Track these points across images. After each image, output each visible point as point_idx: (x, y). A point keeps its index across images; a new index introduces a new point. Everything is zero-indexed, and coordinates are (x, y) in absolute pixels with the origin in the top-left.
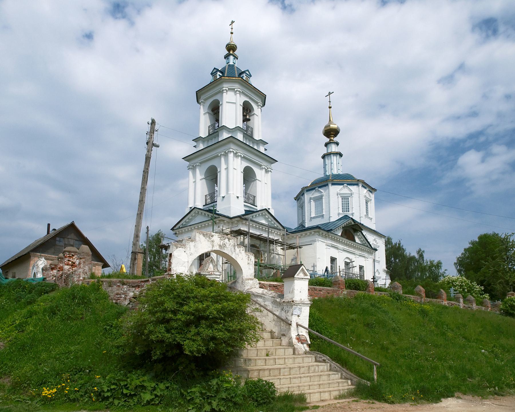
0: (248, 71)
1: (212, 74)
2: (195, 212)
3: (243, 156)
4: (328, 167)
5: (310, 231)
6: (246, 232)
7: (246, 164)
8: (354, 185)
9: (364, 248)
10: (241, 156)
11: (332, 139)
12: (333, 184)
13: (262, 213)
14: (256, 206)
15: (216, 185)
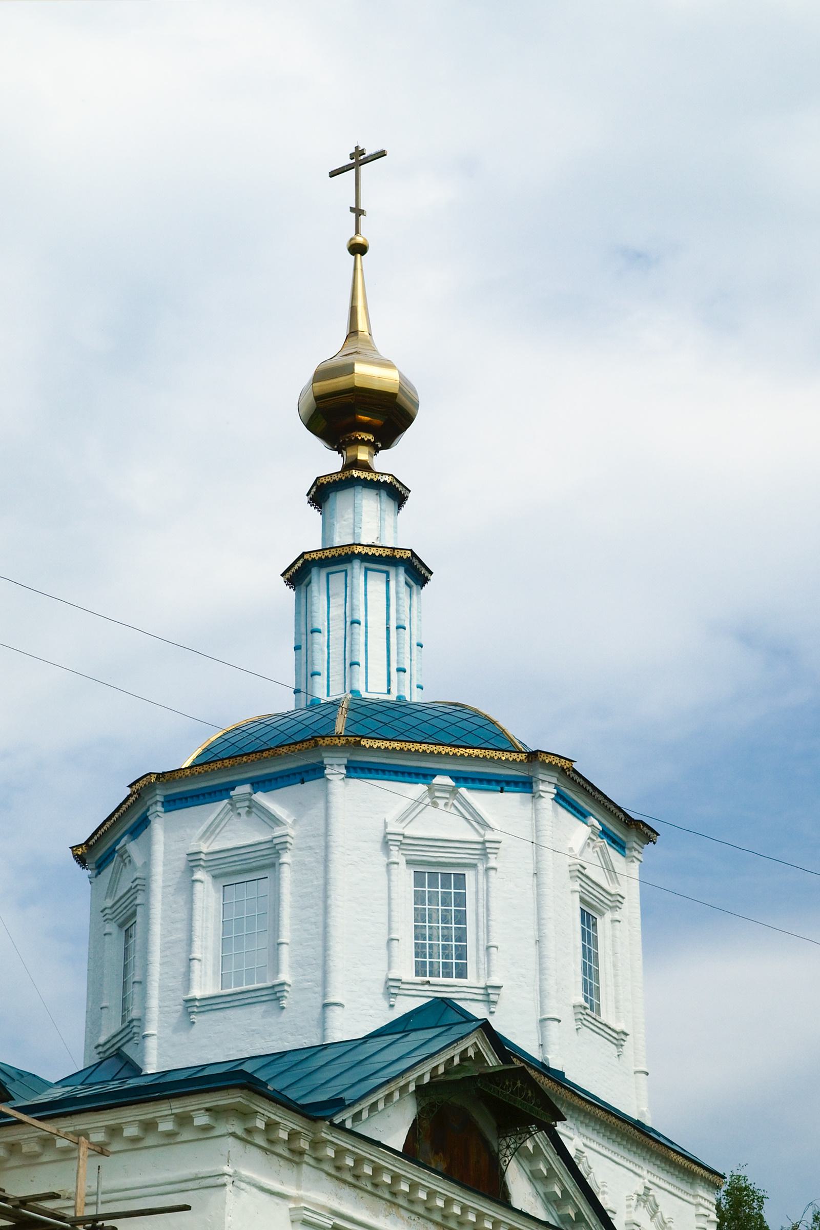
8: (502, 784)
11: (363, 454)
12: (355, 770)
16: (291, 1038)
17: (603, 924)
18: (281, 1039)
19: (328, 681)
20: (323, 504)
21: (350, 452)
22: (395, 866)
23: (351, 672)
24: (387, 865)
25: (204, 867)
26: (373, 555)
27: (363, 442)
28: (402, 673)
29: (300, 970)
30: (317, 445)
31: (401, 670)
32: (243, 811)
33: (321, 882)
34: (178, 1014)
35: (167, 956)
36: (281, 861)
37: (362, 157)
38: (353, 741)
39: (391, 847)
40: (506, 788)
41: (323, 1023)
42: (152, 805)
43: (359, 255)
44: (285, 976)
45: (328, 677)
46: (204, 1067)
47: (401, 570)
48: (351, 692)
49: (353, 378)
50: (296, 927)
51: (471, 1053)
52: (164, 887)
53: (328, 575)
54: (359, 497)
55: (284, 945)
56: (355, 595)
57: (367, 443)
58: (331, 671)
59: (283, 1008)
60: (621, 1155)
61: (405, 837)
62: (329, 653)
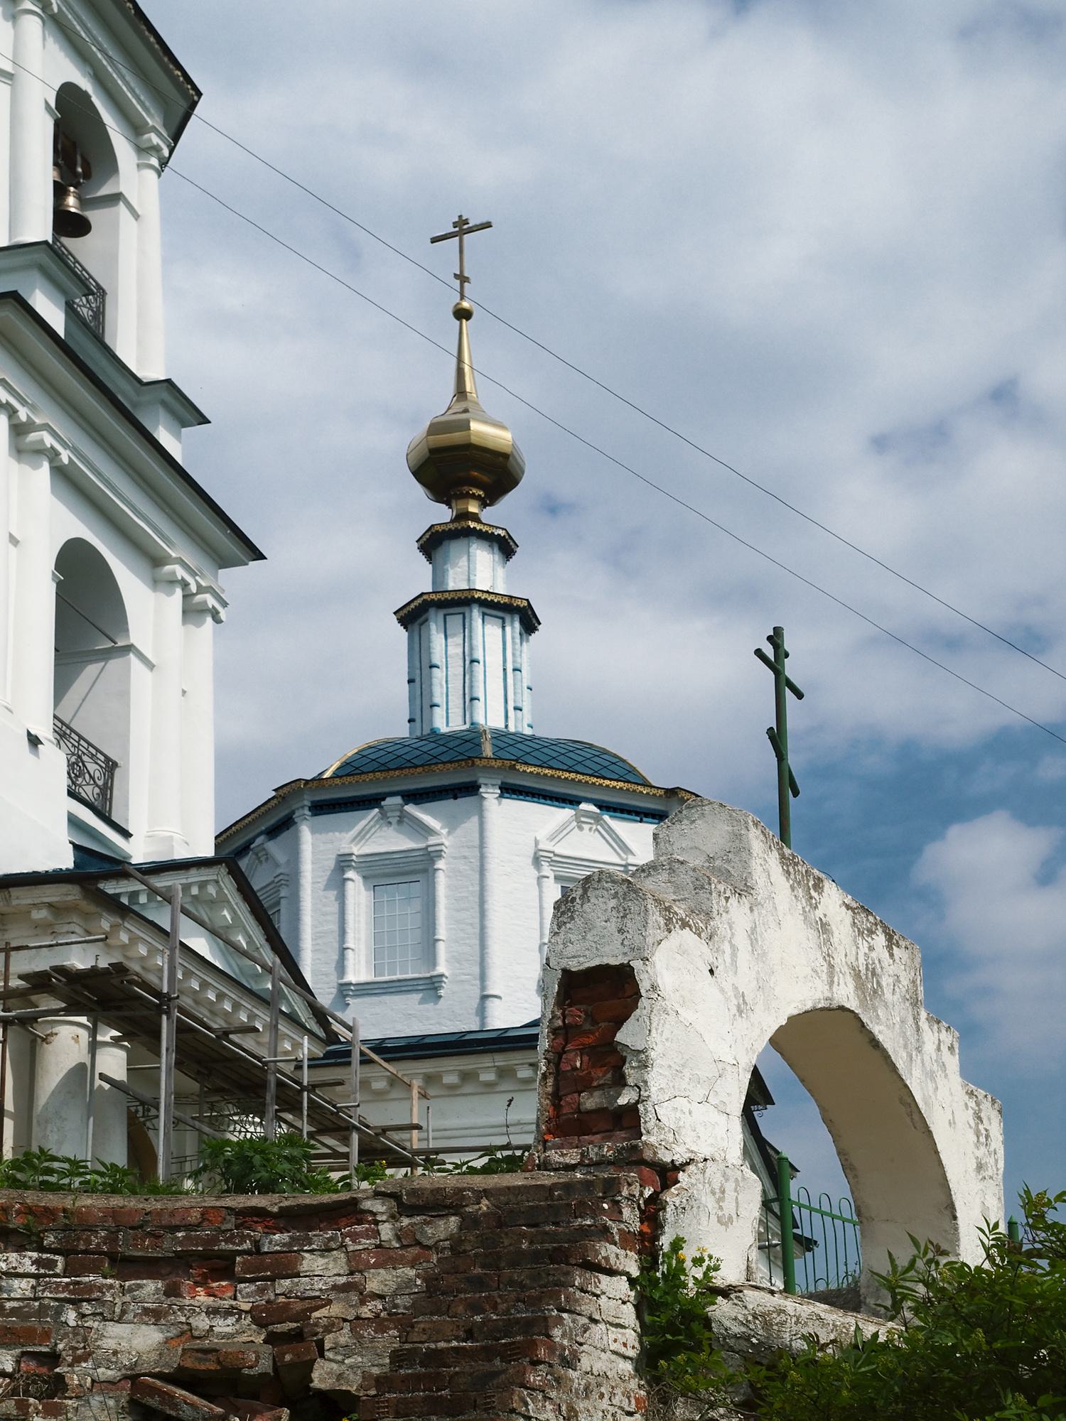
4: (446, 685)
5: (501, 1060)
6: (157, 994)
7: (76, 526)
11: (473, 508)
12: (509, 790)
14: (126, 834)
16: (449, 1023)
18: (439, 1023)
19: (447, 713)
20: (433, 553)
21: (460, 505)
22: (546, 879)
23: (471, 706)
24: (538, 878)
25: (354, 868)
26: (492, 601)
27: (474, 497)
28: (519, 711)
29: (457, 965)
31: (517, 709)
32: (394, 820)
33: (477, 888)
34: (333, 996)
35: (318, 944)
36: (436, 867)
37: (466, 227)
38: (509, 764)
39: (543, 863)
40: (645, 819)
41: (482, 1012)
42: (298, 809)
43: (464, 321)
44: (442, 968)
45: (447, 709)
46: (507, 1030)
47: (517, 618)
48: (472, 724)
49: (469, 436)
50: (452, 926)
52: (313, 883)
53: (445, 616)
54: (474, 546)
55: (441, 942)
56: (474, 637)
57: (478, 498)
58: (450, 703)
59: (441, 997)
61: (555, 855)
62: (447, 688)
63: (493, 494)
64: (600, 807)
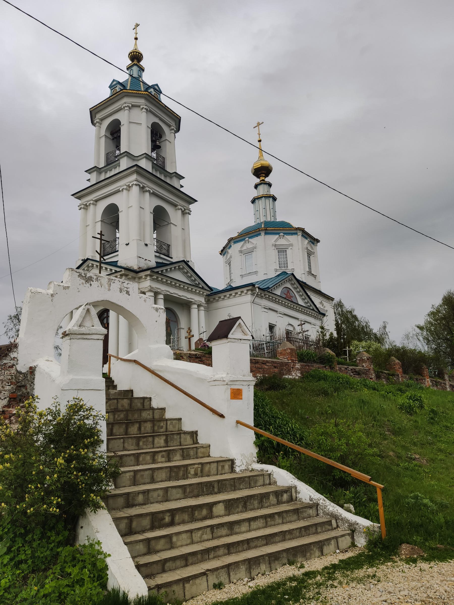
0: (157, 85)
1: (110, 87)
2: (88, 265)
3: (152, 192)
7: (158, 202)
8: (292, 234)
9: (310, 312)
10: (149, 191)
12: (266, 234)
13: (179, 266)
14: (172, 258)
15: (117, 231)
17: (311, 257)
30: (255, 178)
51: (290, 279)
60: (316, 296)
63: (267, 175)
64: (284, 234)
